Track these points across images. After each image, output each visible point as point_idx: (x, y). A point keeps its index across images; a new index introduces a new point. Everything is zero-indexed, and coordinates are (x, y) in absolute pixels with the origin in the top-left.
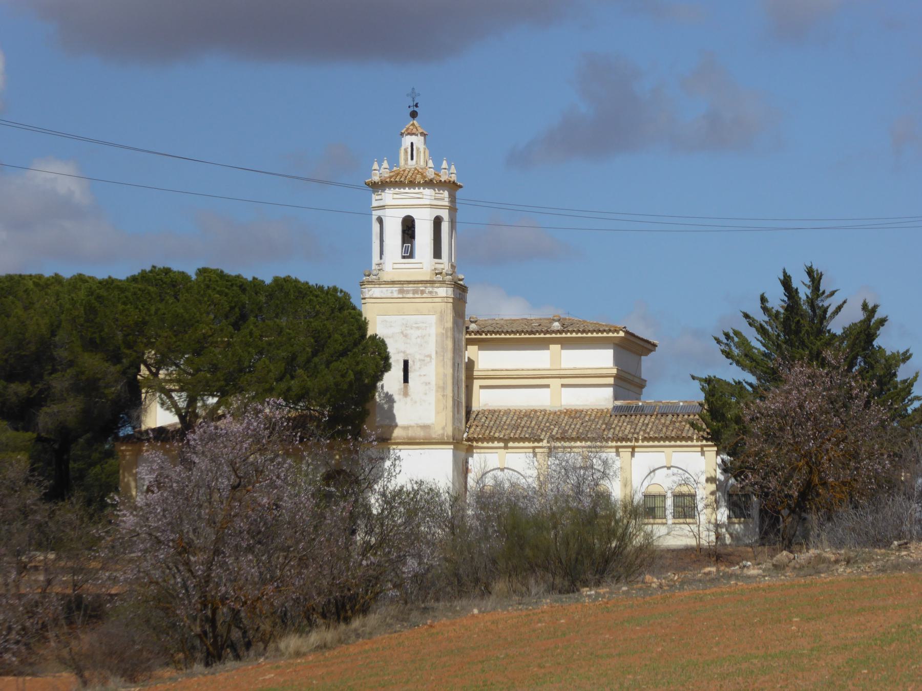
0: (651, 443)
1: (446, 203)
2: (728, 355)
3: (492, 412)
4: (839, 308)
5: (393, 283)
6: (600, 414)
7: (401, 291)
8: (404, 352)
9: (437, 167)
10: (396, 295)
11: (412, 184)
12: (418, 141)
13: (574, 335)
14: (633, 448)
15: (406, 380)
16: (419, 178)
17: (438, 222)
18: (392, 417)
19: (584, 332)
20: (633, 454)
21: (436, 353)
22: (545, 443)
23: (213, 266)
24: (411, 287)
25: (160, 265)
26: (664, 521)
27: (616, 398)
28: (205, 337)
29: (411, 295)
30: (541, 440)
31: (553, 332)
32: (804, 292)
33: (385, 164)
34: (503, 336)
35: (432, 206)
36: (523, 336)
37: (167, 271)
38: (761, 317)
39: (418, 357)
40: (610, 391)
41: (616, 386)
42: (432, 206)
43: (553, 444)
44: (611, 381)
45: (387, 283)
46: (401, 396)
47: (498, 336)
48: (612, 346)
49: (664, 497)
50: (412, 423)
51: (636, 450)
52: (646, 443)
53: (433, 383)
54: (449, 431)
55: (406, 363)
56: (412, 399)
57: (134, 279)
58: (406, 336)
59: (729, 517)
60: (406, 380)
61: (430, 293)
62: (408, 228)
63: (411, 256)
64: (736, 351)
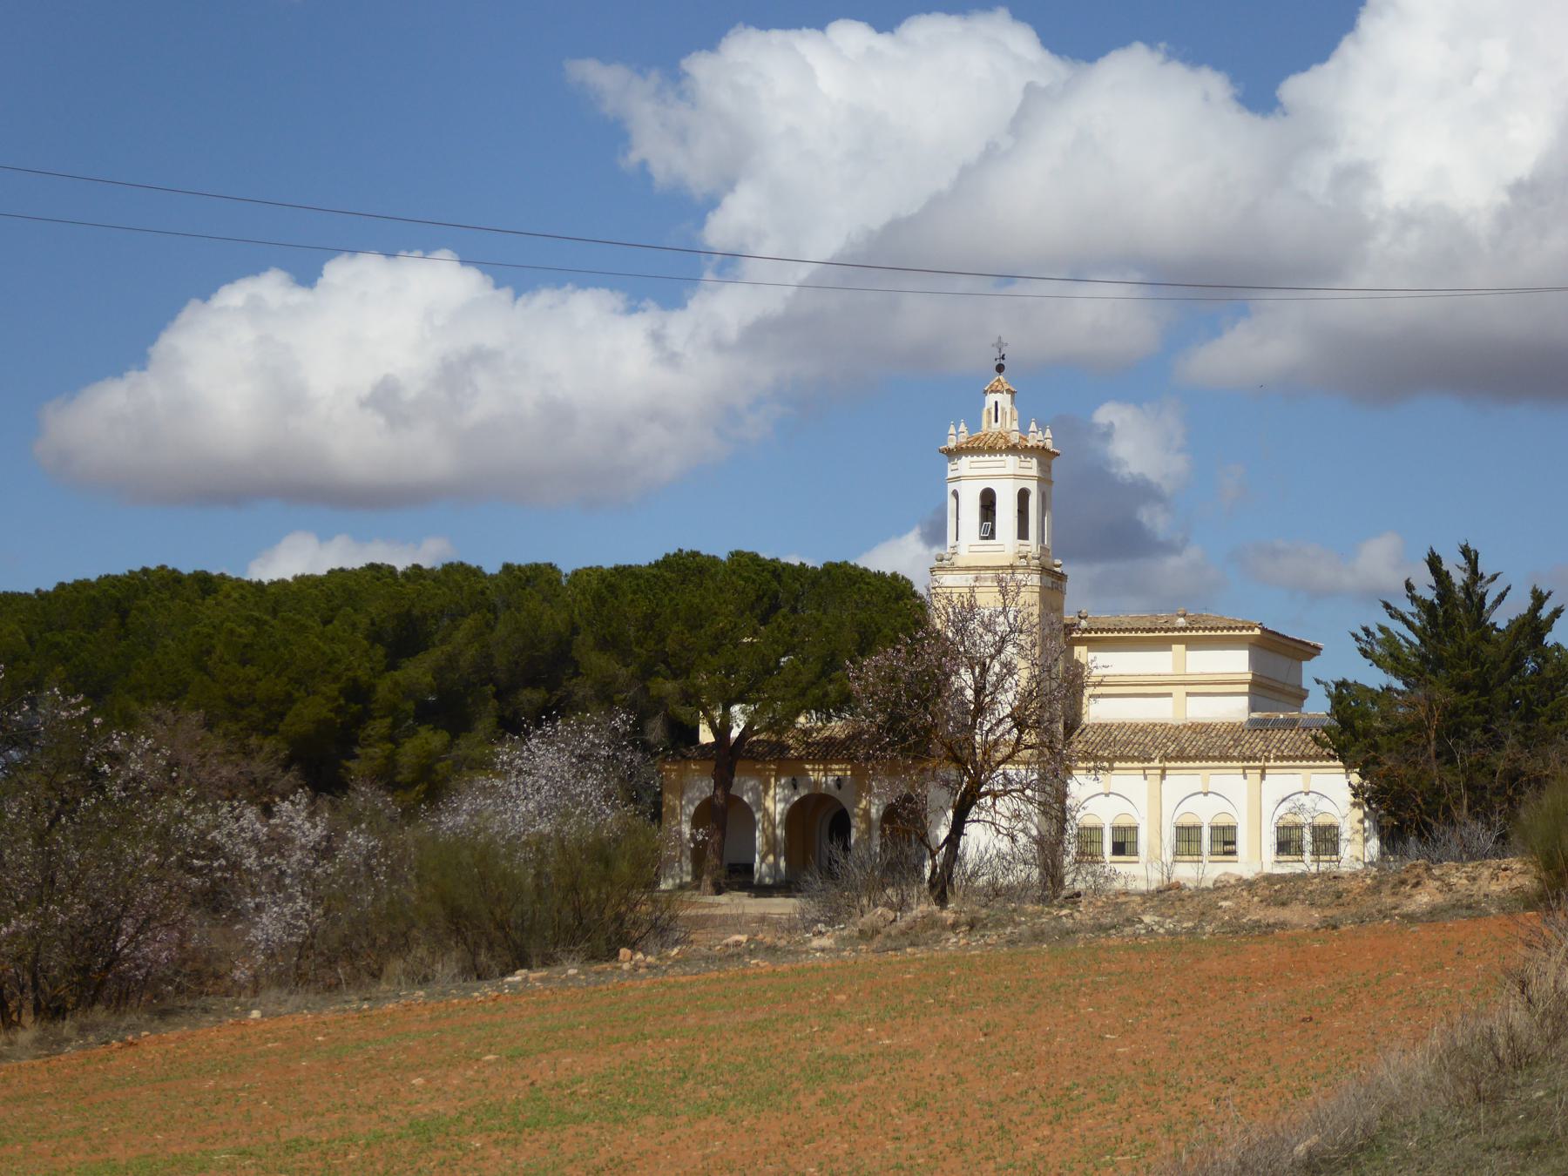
0: (1285, 763)
1: (1034, 472)
2: (1365, 654)
3: (1102, 726)
4: (1502, 596)
5: (968, 568)
6: (1232, 729)
9: (1024, 429)
11: (992, 450)
12: (1004, 400)
13: (1200, 633)
14: (1263, 769)
16: (1001, 444)
17: (1023, 496)
19: (1230, 628)
20: (1263, 777)
22: (1156, 763)
23: (747, 549)
25: (687, 549)
27: (1253, 708)
28: (723, 632)
31: (1175, 629)
32: (1458, 577)
33: (962, 427)
35: (1016, 477)
37: (695, 554)
38: (1407, 607)
40: (1244, 701)
41: (1251, 694)
42: (1016, 477)
43: (1167, 764)
44: (1246, 688)
45: (960, 569)
52: (1279, 763)
57: (657, 565)
59: (1383, 854)
62: (988, 502)
63: (992, 536)
64: (1378, 650)
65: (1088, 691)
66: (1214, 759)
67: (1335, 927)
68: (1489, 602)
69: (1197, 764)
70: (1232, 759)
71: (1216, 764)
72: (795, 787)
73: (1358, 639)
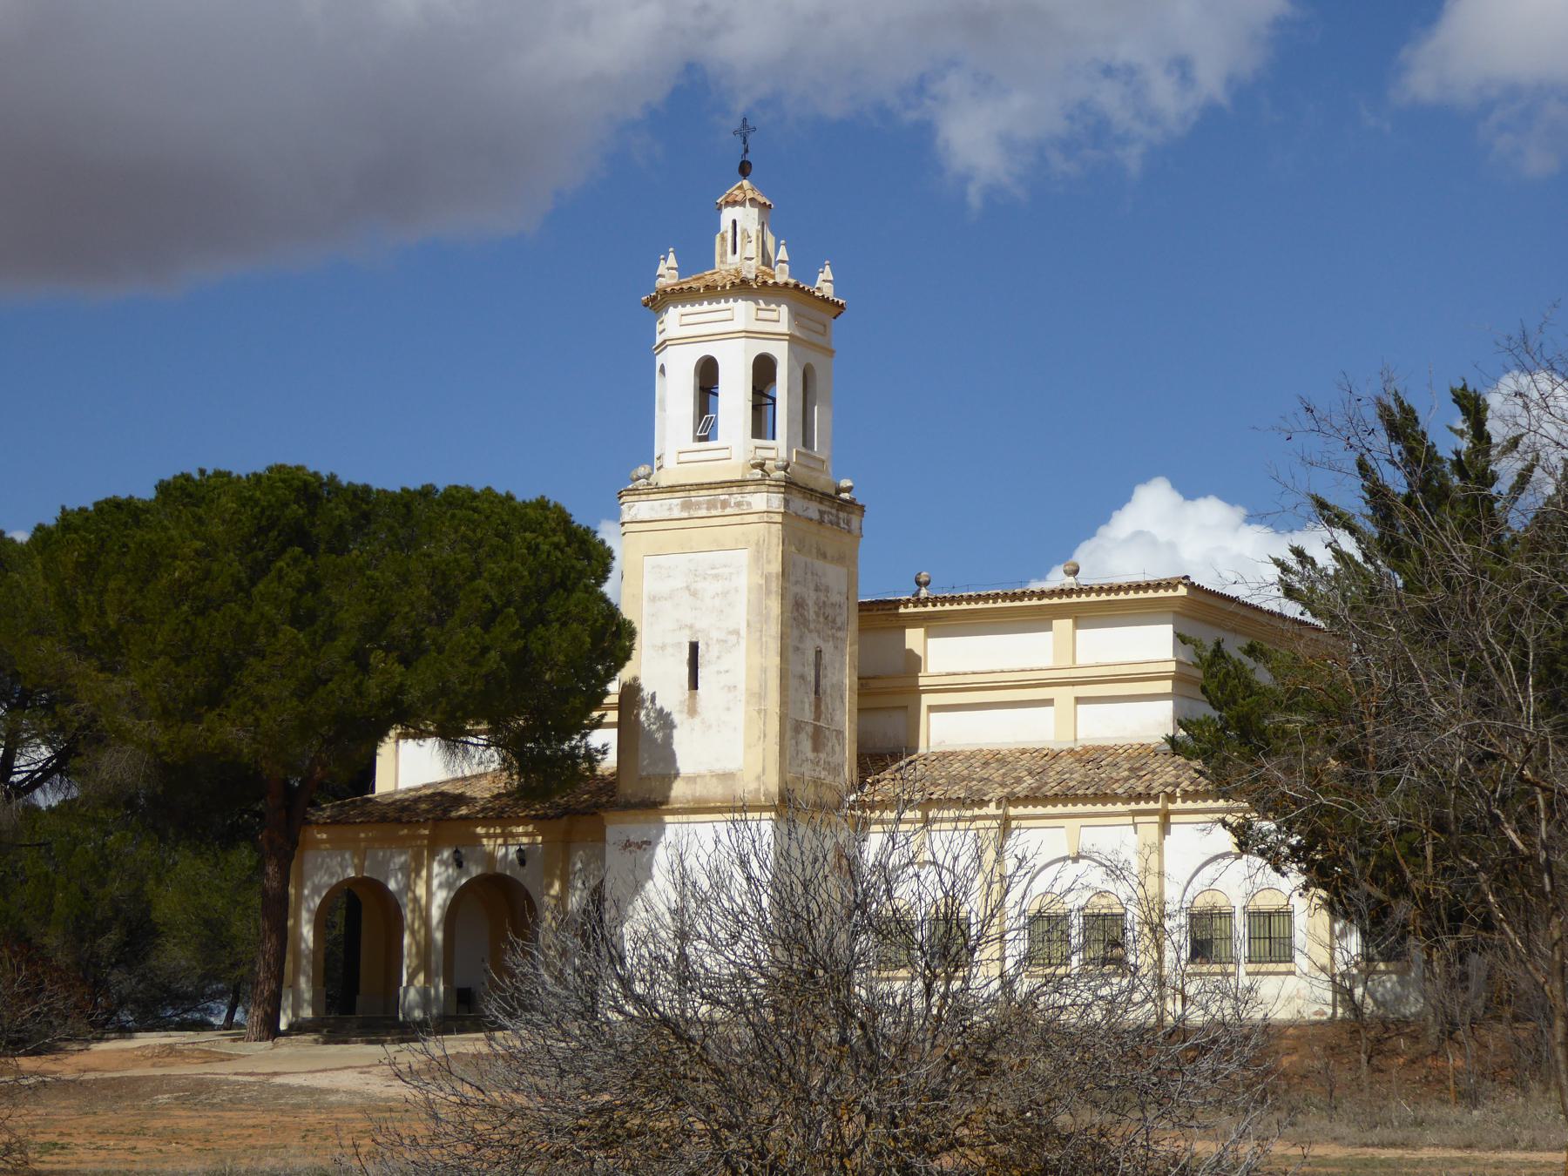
1: (783, 327)
5: (672, 489)
7: (686, 506)
8: (691, 627)
10: (676, 513)
14: (1166, 816)
15: (694, 683)
17: (764, 369)
18: (671, 758)
20: (1165, 828)
21: (748, 625)
22: (992, 809)
24: (702, 496)
26: (1291, 966)
29: (703, 513)
30: (983, 803)
34: (964, 606)
35: (750, 334)
36: (1000, 604)
39: (715, 635)
42: (750, 334)
43: (1012, 811)
44: (1166, 686)
46: (685, 716)
47: (955, 607)
48: (1171, 617)
49: (1230, 915)
50: (703, 770)
51: (1173, 818)
52: (1190, 805)
53: (742, 687)
54: (772, 783)
55: (694, 648)
56: (703, 722)
58: (694, 594)
59: (1368, 959)
60: (694, 683)
61: (738, 504)
62: (707, 374)
65: (927, 700)
66: (1085, 799)
67: (987, 1069)
68: (1503, 486)
69: (1060, 809)
70: (1115, 798)
71: (1089, 808)
72: (459, 864)
73: (1284, 568)
